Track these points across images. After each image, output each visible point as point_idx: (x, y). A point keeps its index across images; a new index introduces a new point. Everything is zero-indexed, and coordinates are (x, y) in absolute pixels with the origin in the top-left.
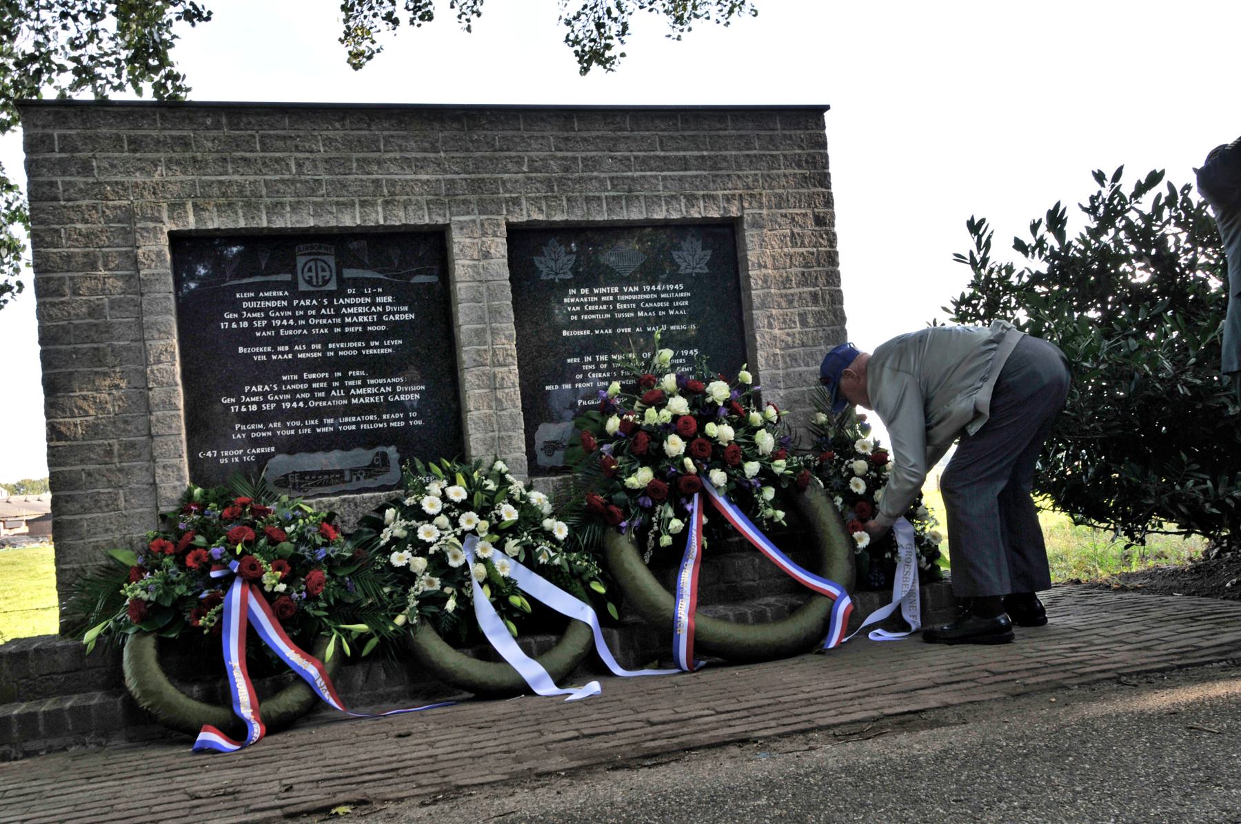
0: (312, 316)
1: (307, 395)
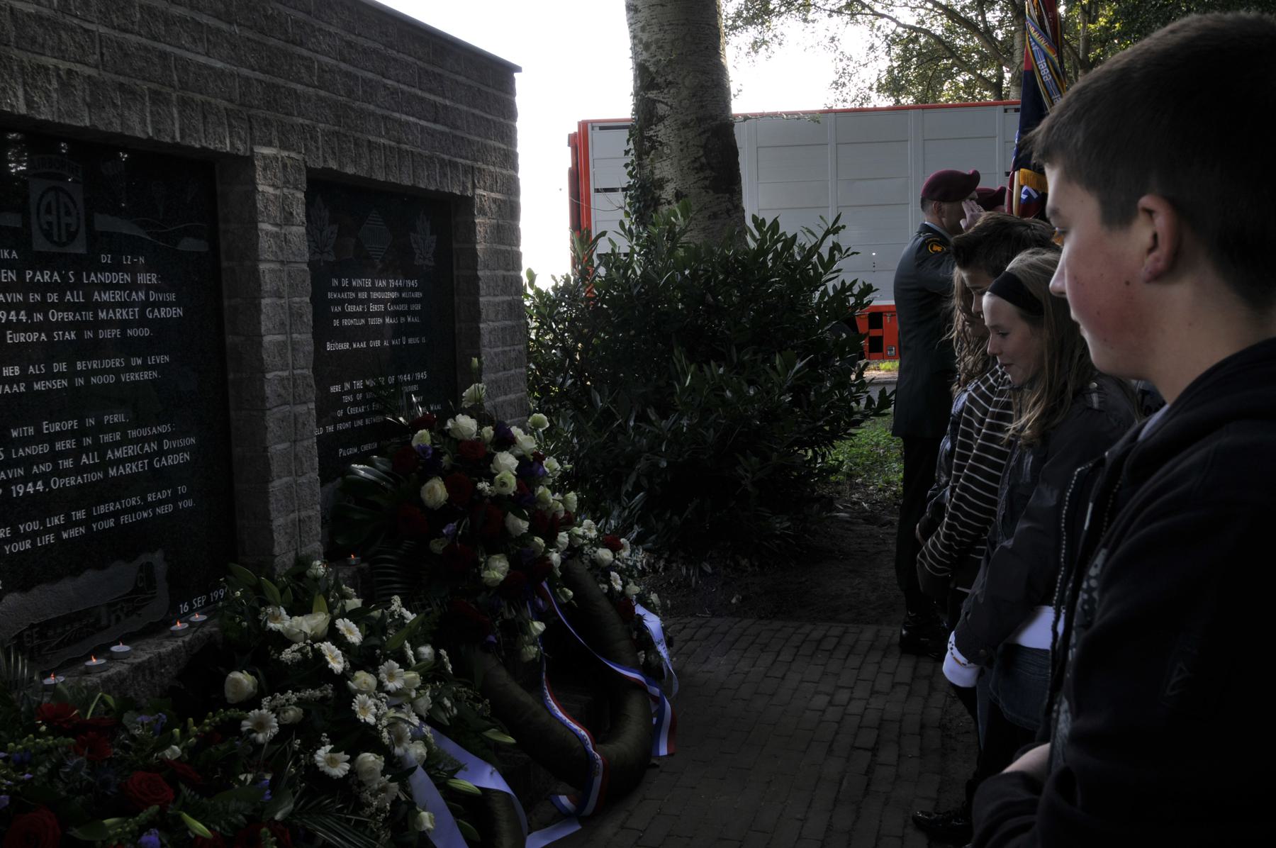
0: (53, 305)
1: (46, 467)
